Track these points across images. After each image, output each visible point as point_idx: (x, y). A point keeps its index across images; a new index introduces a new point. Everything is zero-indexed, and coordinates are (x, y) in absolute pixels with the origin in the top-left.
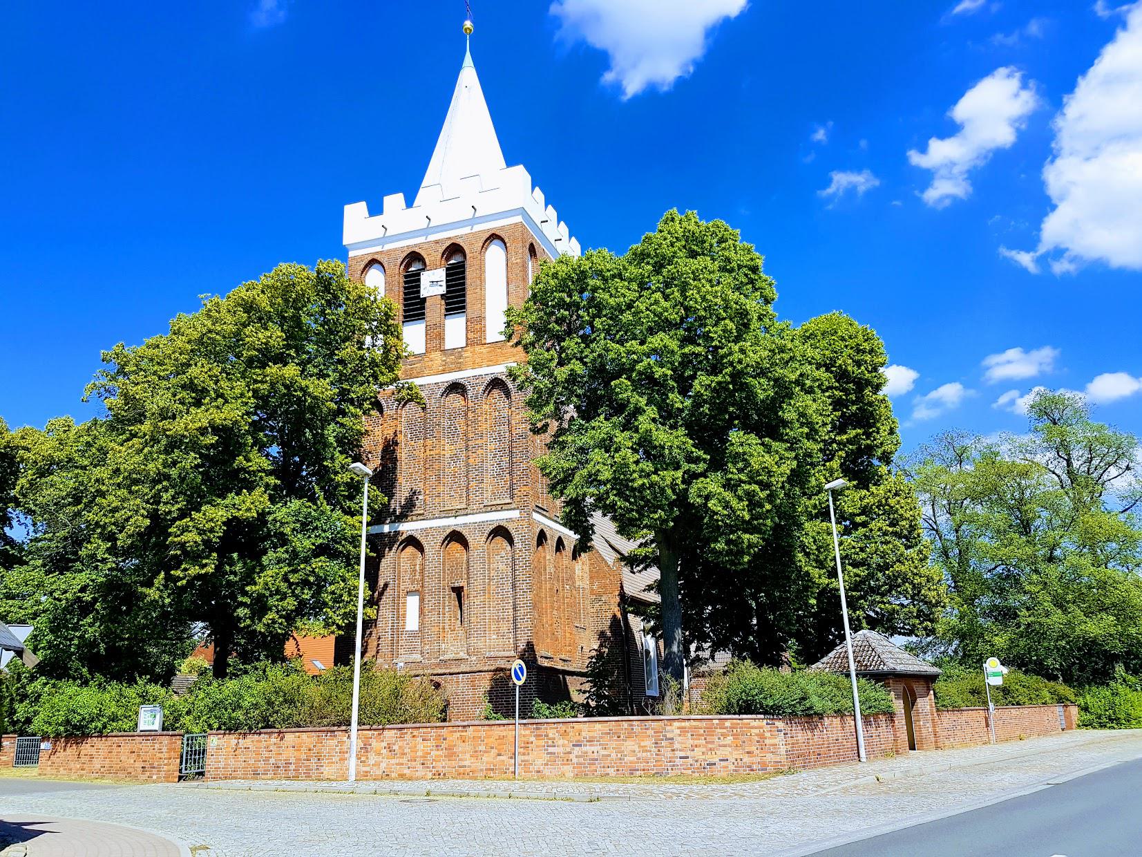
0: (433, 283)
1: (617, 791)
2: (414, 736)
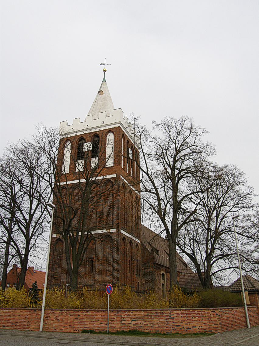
0: (87, 146)
1: (150, 341)
2: (67, 314)
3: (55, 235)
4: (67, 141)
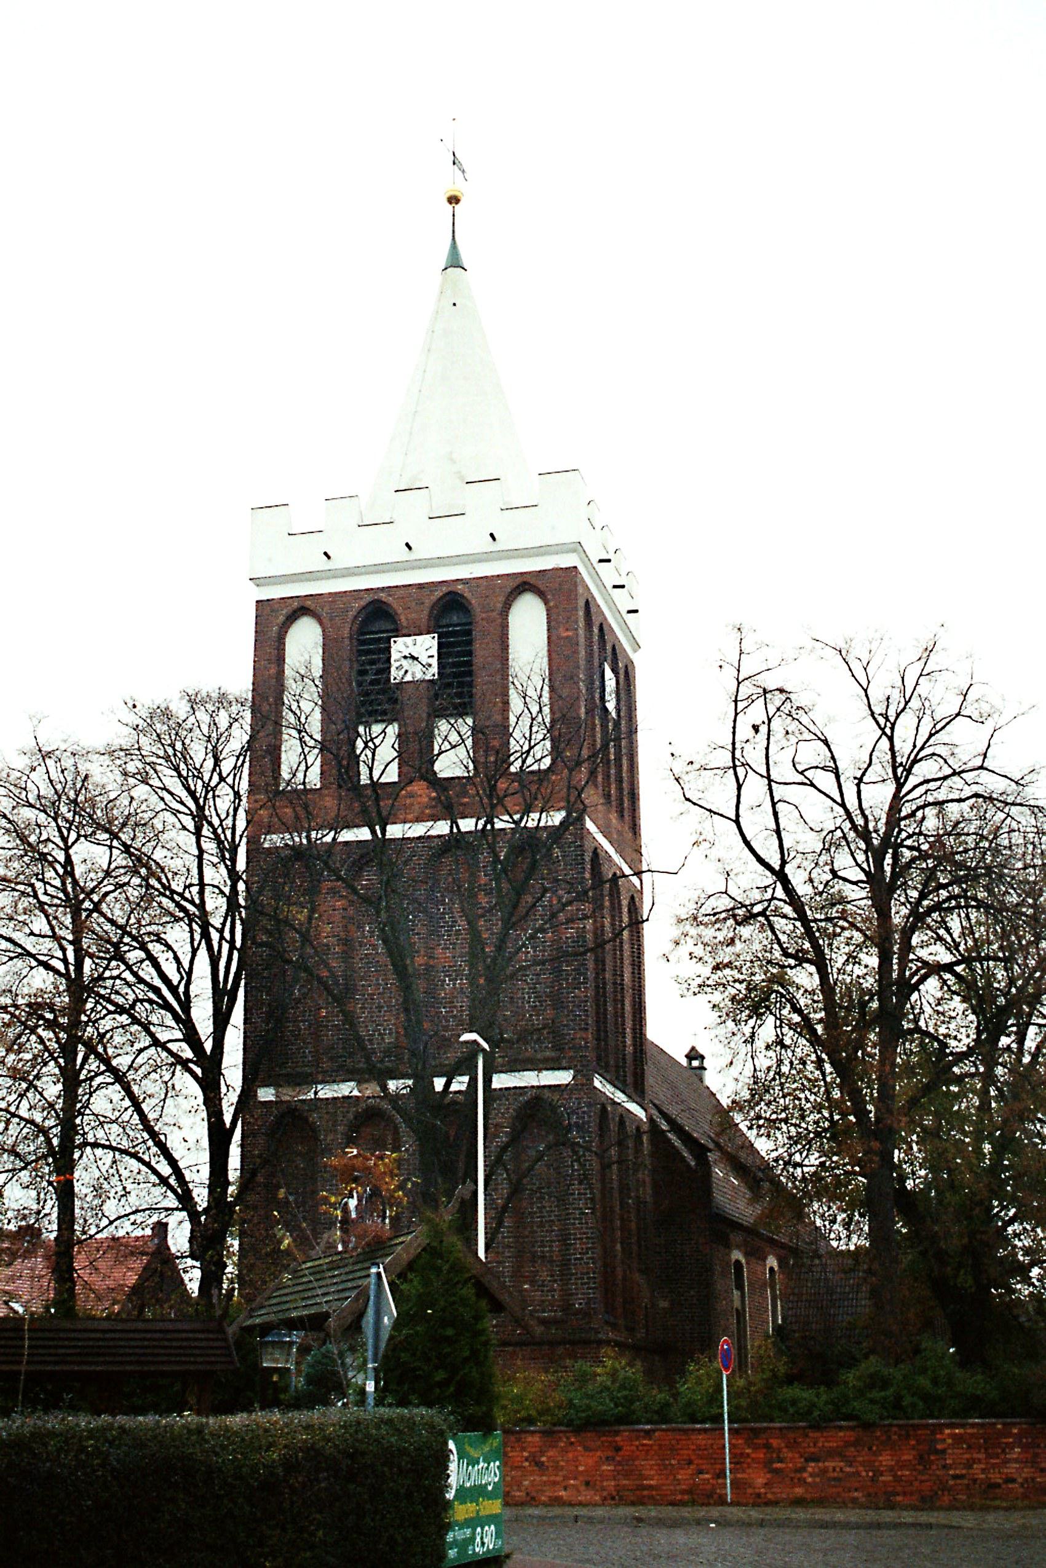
3: (272, 1091)
4: (293, 617)
